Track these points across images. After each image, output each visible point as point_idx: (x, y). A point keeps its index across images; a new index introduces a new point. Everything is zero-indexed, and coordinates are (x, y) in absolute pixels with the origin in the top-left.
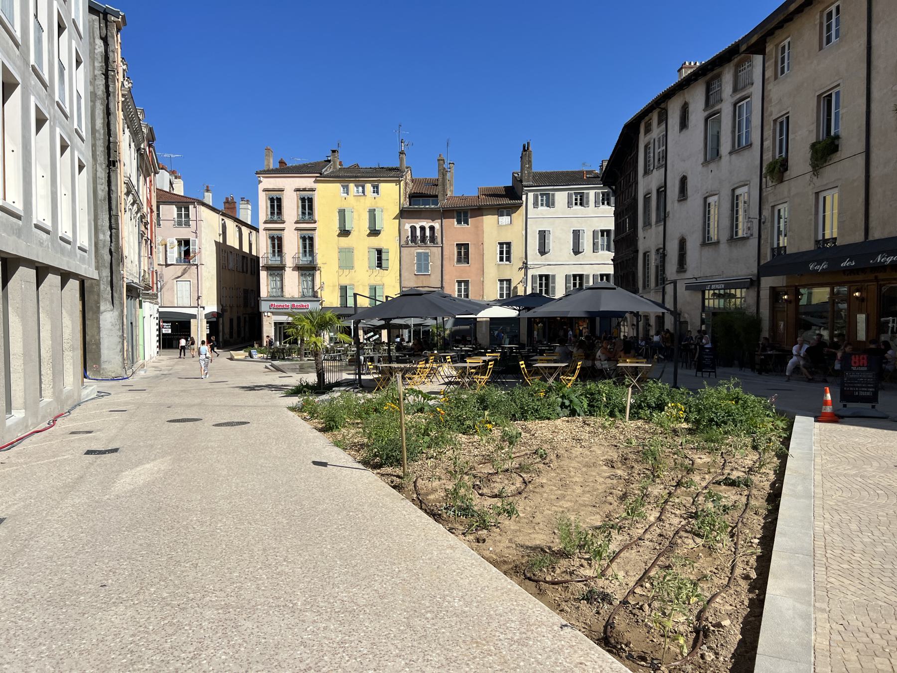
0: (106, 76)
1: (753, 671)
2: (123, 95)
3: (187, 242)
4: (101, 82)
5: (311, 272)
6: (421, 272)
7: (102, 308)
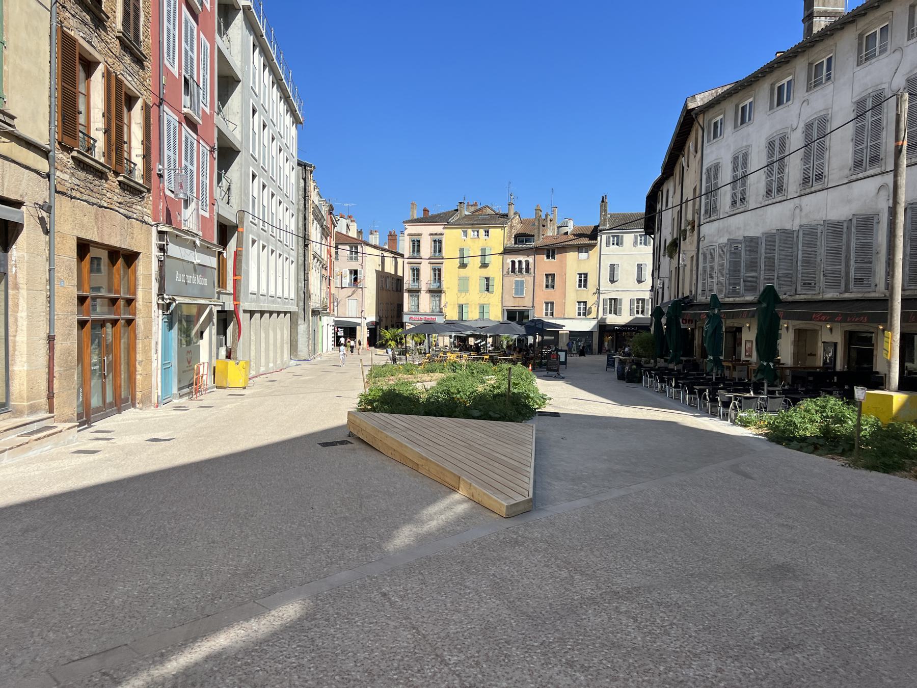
0: (305, 198)
2: (313, 208)
3: (356, 272)
4: (302, 202)
5: (439, 294)
6: (518, 294)
7: (299, 323)
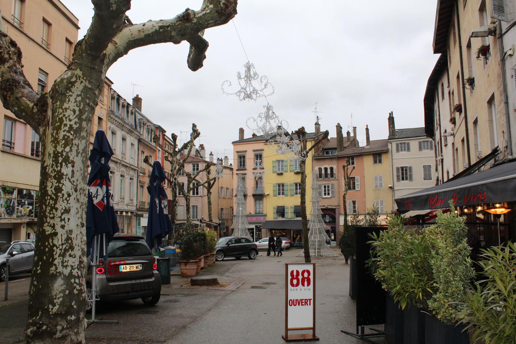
1: (482, 1)
